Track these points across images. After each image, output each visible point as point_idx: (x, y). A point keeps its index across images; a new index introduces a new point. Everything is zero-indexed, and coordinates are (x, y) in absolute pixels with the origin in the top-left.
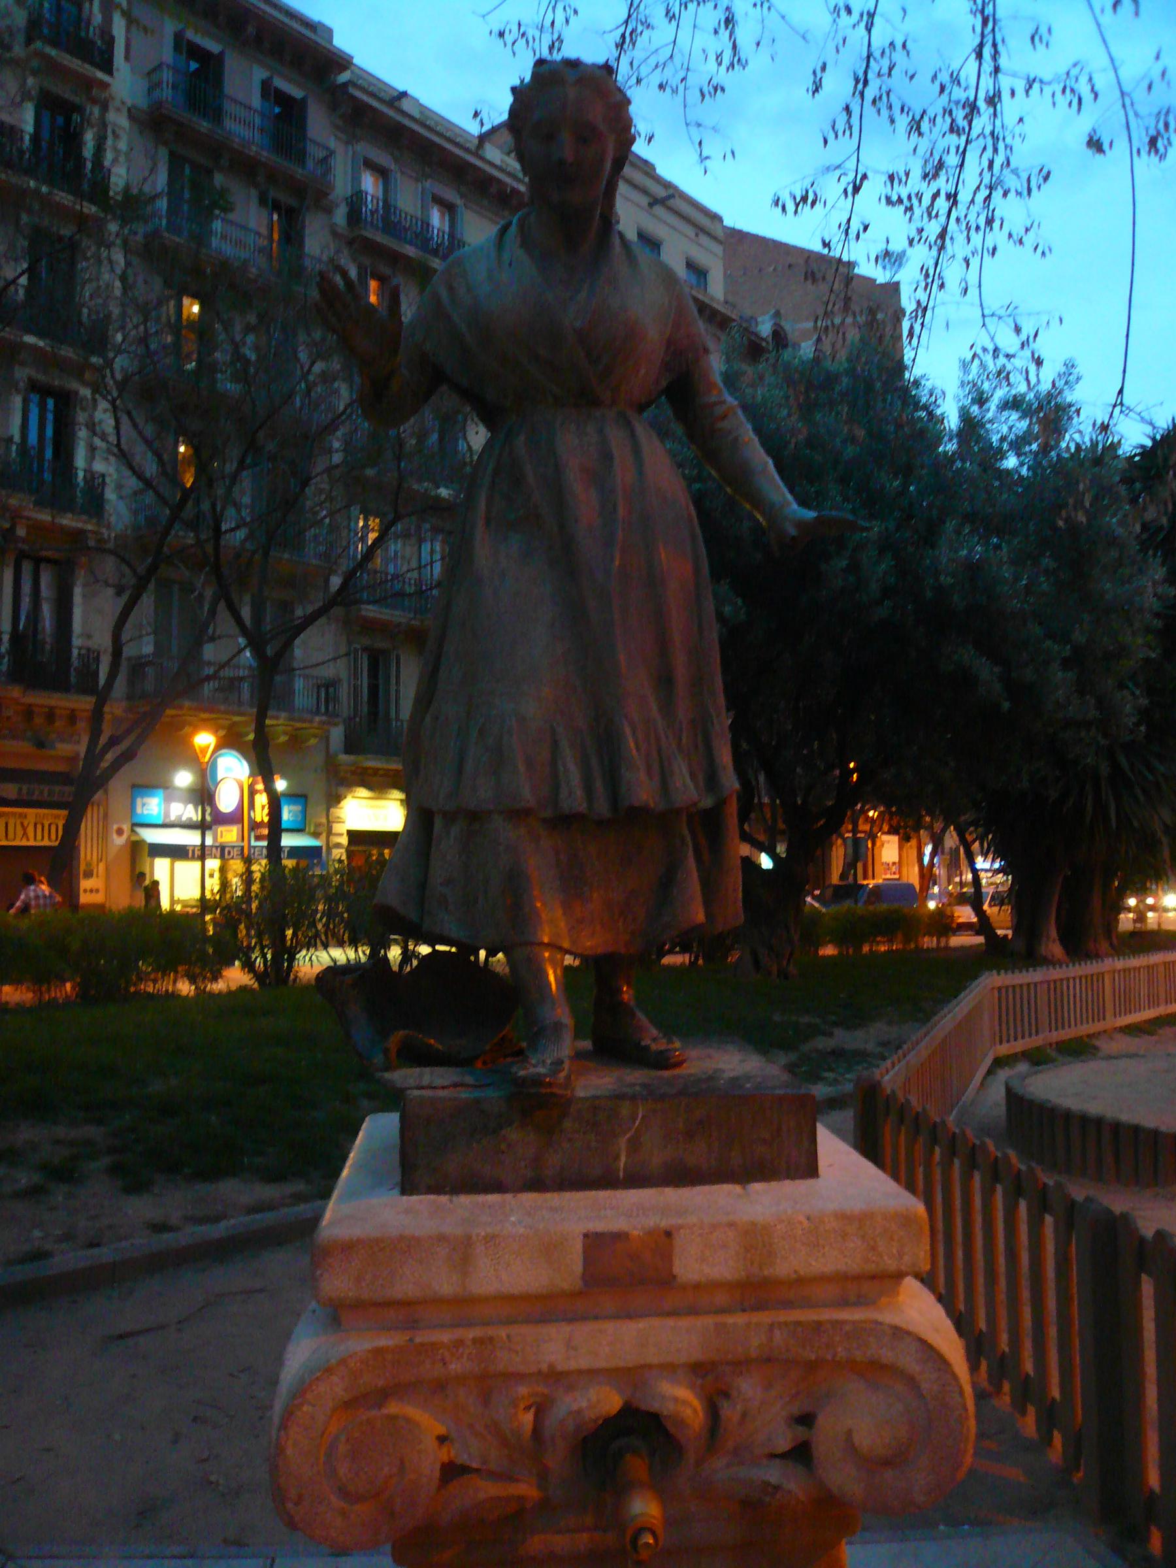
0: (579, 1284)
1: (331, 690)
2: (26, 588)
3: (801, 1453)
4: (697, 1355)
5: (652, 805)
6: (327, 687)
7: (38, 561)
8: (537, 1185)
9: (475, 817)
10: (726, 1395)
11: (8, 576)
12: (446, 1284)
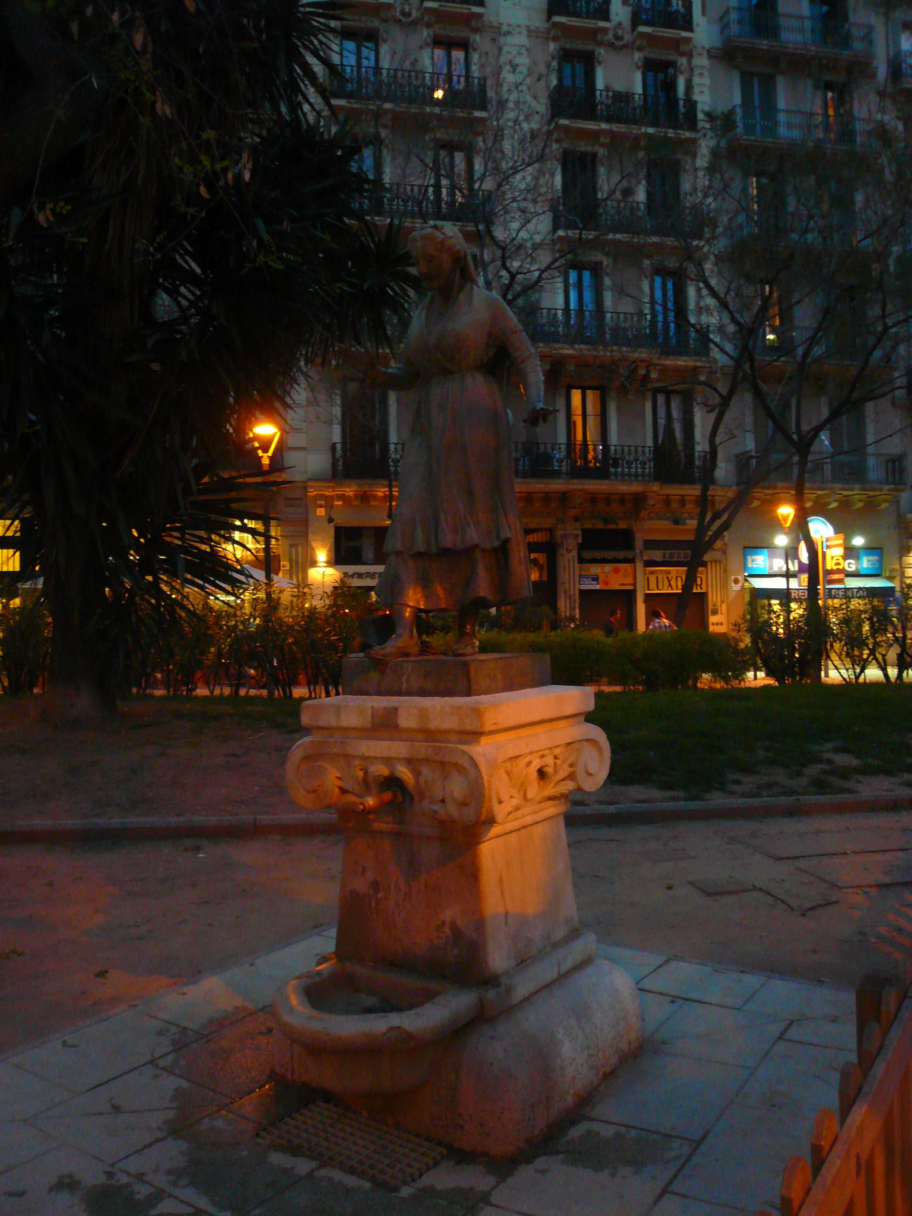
2: (662, 413)
6: (893, 461)
8: (379, 693)
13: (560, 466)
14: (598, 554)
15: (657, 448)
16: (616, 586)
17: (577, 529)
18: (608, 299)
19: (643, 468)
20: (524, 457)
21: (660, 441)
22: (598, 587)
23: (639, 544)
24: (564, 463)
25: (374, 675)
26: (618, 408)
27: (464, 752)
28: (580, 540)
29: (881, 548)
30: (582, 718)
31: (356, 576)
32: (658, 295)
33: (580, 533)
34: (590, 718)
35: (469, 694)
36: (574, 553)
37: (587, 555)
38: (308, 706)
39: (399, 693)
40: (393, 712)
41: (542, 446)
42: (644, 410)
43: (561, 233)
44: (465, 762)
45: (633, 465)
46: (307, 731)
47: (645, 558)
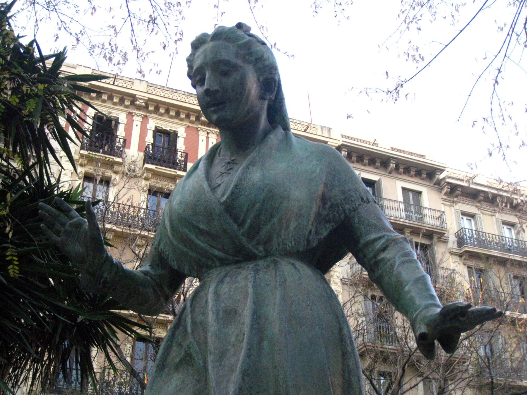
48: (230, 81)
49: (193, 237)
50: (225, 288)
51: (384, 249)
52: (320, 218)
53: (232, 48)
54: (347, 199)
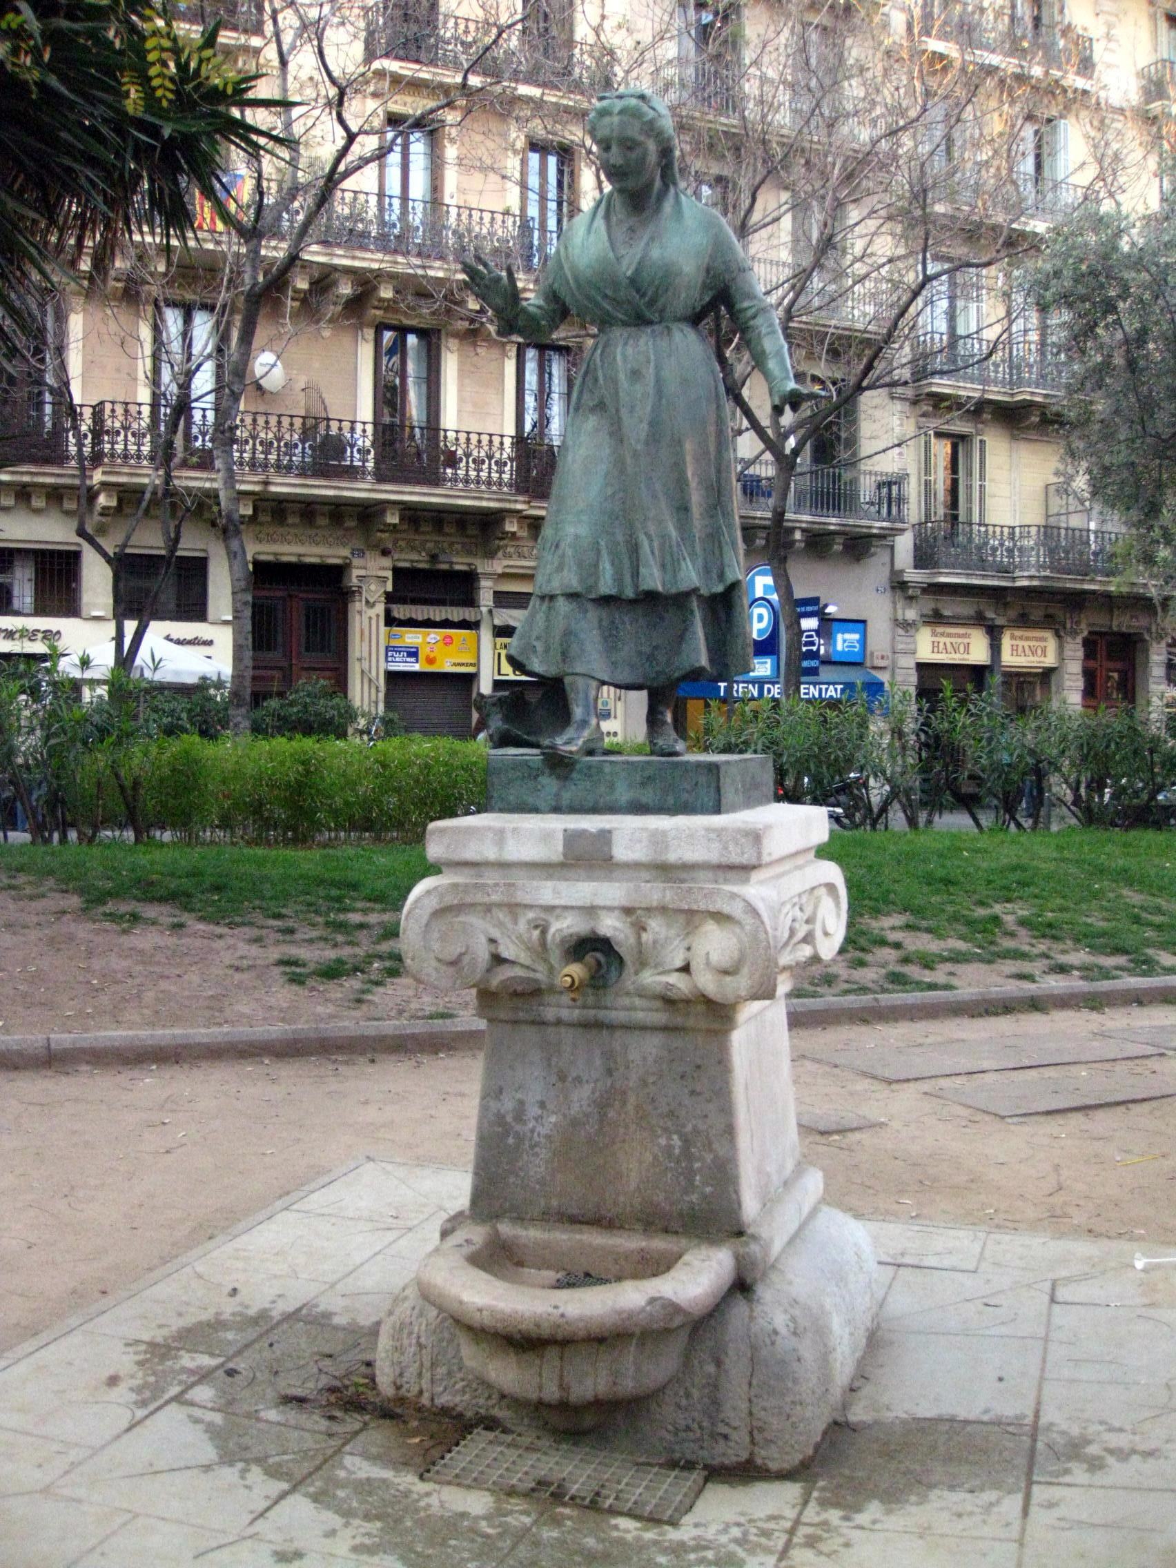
0: (561, 858)
1: (895, 488)
2: (531, 378)
3: (686, 969)
4: (625, 903)
5: (660, 589)
6: (889, 484)
7: (542, 348)
8: (557, 810)
9: (552, 598)
10: (644, 929)
11: (510, 367)
12: (491, 853)
13: (364, 461)
14: (421, 612)
15: (520, 440)
16: (446, 666)
17: (384, 569)
18: (451, 178)
19: (501, 472)
20: (303, 442)
21: (528, 427)
22: (416, 667)
23: (486, 598)
24: (507, 468)
25: (549, 784)
26: (461, 364)
27: (734, 896)
28: (389, 588)
29: (864, 622)
30: (813, 853)
31: (40, 636)
32: (534, 181)
33: (389, 574)
34: (823, 852)
35: (717, 810)
36: (380, 609)
37: (400, 612)
38: (443, 831)
39: (612, 809)
40: (605, 837)
41: (334, 426)
42: (502, 374)
43: (376, 65)
44: (736, 909)
45: (485, 466)
46: (433, 869)
47: (497, 622)
48: (633, 156)
49: (599, 298)
50: (630, 350)
51: (754, 317)
52: (705, 287)
53: (637, 124)
54: (728, 270)
